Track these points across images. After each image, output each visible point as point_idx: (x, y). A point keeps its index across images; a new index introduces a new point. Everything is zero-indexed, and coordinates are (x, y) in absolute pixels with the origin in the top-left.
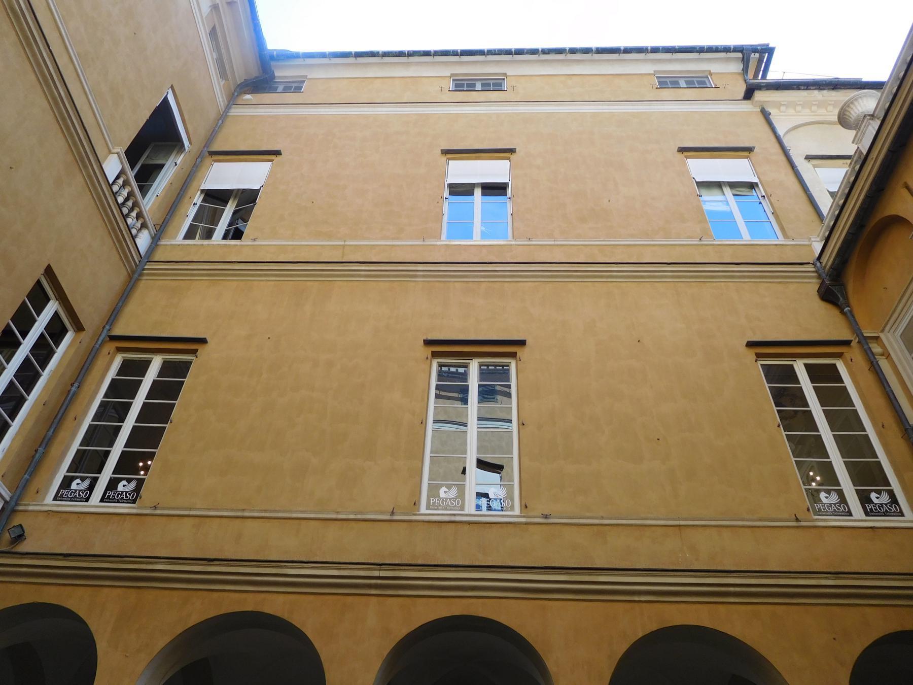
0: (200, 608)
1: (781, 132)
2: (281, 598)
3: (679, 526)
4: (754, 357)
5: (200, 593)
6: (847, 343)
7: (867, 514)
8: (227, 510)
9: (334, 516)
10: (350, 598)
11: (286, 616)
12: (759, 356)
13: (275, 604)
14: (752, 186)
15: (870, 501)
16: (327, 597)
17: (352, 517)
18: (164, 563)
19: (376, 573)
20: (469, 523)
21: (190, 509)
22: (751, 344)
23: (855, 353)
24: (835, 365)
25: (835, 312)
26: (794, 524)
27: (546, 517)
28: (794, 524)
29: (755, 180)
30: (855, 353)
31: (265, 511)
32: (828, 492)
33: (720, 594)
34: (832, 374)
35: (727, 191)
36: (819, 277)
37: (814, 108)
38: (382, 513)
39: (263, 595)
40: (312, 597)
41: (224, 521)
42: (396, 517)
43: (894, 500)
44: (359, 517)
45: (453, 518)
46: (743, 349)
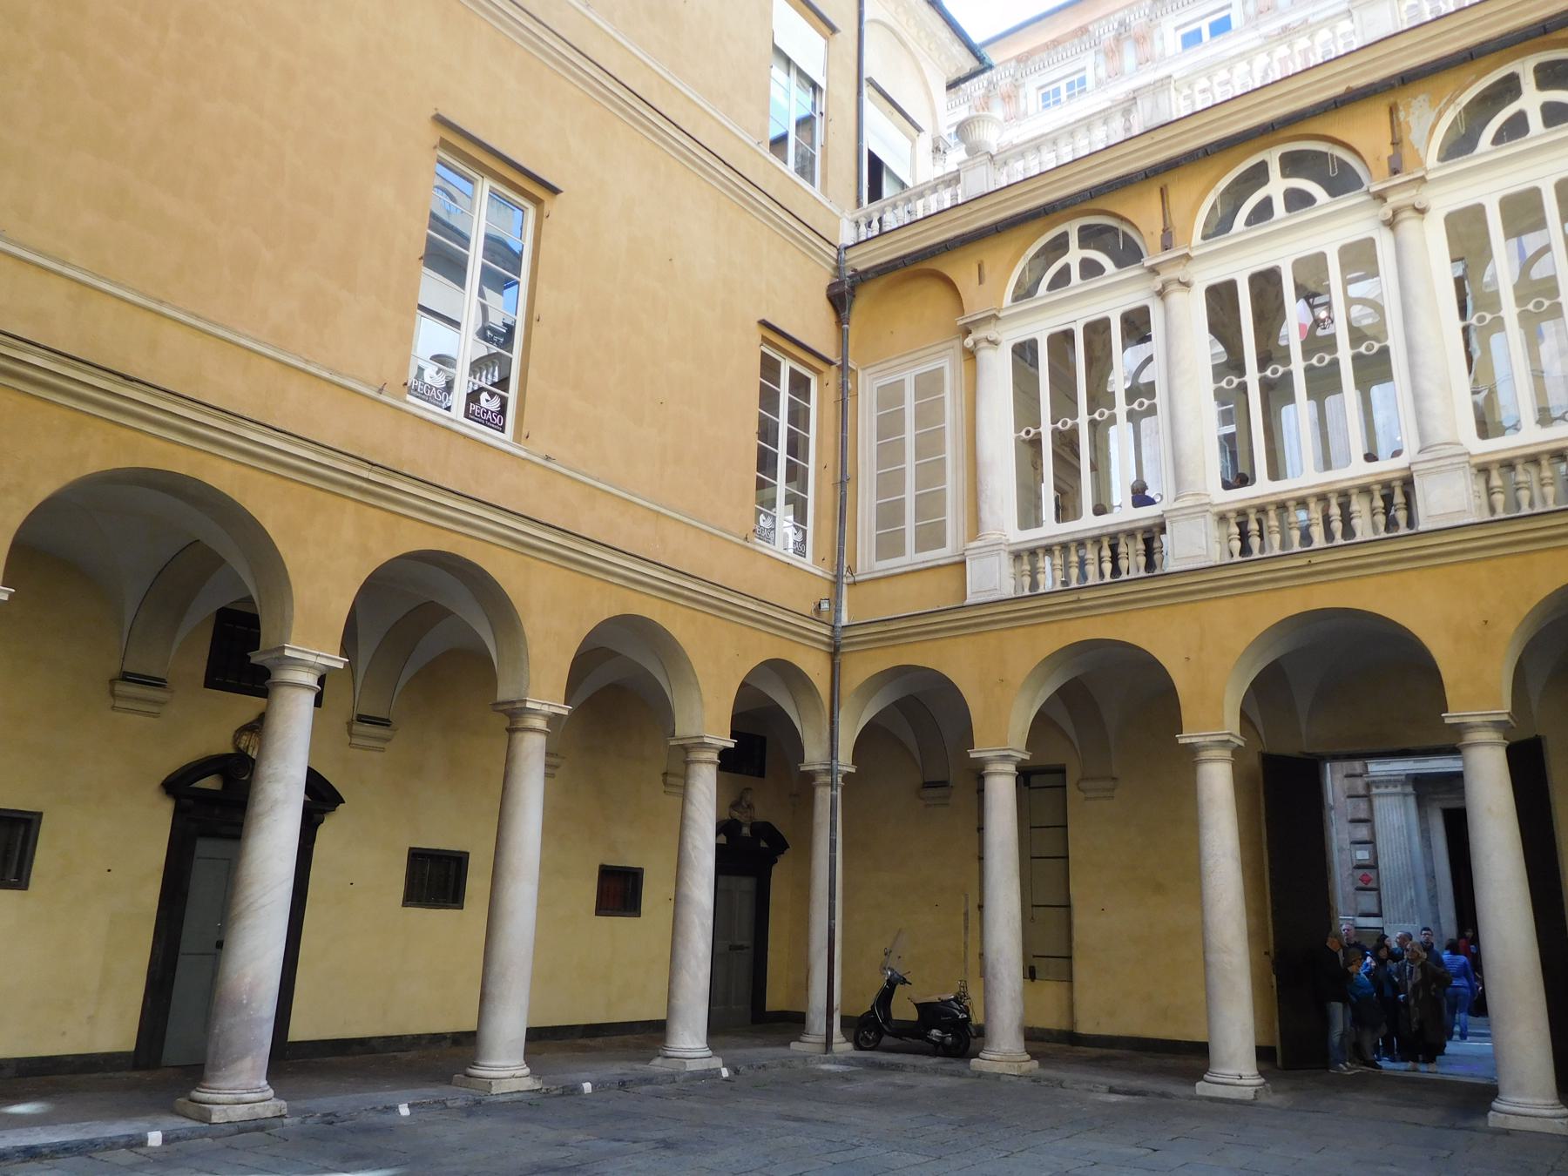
0: (102, 451)
1: (866, 17)
2: (228, 467)
3: (658, 513)
4: (436, 141)
5: (99, 423)
6: (829, 363)
7: (467, 416)
8: (133, 290)
9: (302, 365)
10: (321, 495)
11: (236, 497)
12: (765, 340)
13: (222, 475)
14: (815, 86)
15: (477, 401)
16: (291, 484)
17: (325, 374)
18: (39, 355)
19: (365, 474)
20: (466, 436)
21: (217, 324)
22: (765, 324)
23: (831, 375)
24: (808, 380)
25: (832, 317)
26: (741, 542)
27: (548, 458)
28: (741, 542)
29: (822, 82)
30: (831, 375)
31: (198, 317)
32: (492, 395)
33: (674, 593)
34: (800, 385)
35: (793, 73)
36: (838, 268)
37: (900, 10)
38: (367, 384)
39: (203, 456)
40: (271, 479)
41: (126, 306)
42: (383, 397)
43: (502, 411)
44: (335, 378)
45: (449, 424)
46: (754, 324)
